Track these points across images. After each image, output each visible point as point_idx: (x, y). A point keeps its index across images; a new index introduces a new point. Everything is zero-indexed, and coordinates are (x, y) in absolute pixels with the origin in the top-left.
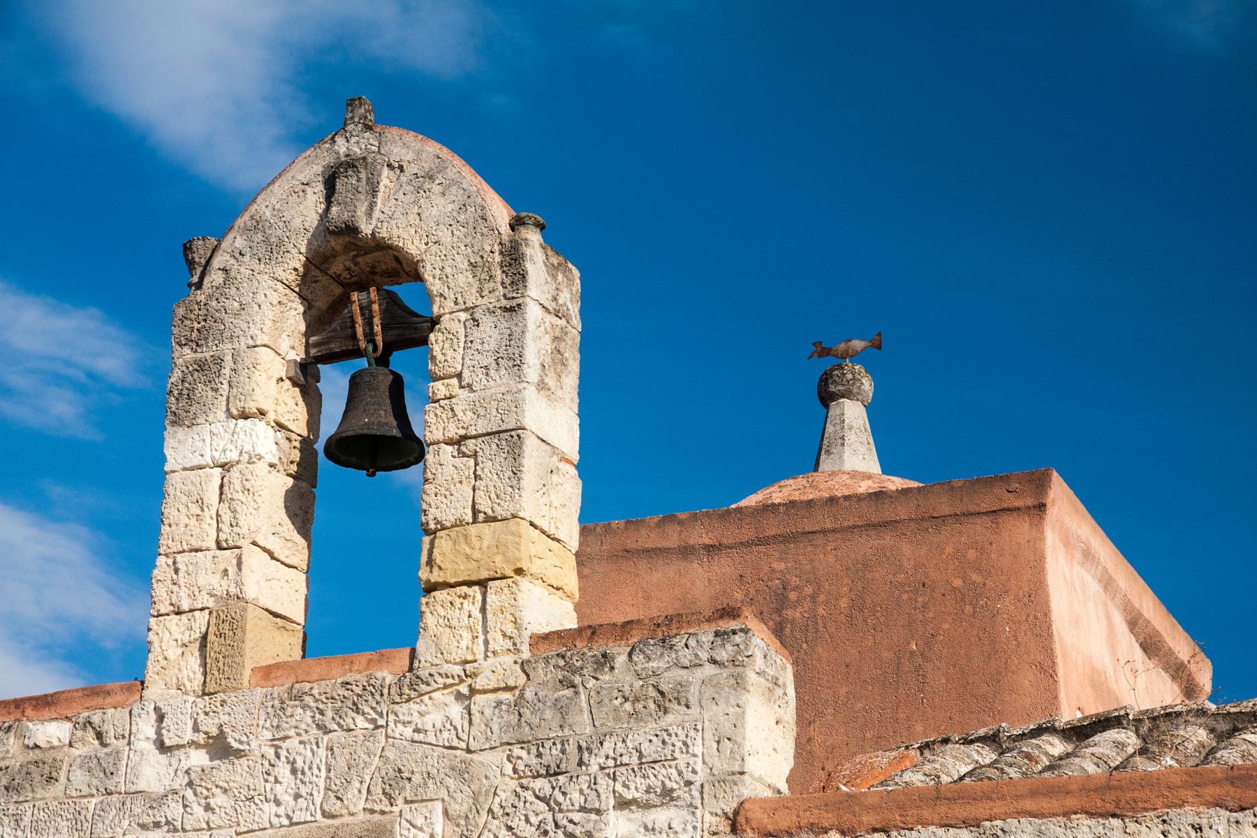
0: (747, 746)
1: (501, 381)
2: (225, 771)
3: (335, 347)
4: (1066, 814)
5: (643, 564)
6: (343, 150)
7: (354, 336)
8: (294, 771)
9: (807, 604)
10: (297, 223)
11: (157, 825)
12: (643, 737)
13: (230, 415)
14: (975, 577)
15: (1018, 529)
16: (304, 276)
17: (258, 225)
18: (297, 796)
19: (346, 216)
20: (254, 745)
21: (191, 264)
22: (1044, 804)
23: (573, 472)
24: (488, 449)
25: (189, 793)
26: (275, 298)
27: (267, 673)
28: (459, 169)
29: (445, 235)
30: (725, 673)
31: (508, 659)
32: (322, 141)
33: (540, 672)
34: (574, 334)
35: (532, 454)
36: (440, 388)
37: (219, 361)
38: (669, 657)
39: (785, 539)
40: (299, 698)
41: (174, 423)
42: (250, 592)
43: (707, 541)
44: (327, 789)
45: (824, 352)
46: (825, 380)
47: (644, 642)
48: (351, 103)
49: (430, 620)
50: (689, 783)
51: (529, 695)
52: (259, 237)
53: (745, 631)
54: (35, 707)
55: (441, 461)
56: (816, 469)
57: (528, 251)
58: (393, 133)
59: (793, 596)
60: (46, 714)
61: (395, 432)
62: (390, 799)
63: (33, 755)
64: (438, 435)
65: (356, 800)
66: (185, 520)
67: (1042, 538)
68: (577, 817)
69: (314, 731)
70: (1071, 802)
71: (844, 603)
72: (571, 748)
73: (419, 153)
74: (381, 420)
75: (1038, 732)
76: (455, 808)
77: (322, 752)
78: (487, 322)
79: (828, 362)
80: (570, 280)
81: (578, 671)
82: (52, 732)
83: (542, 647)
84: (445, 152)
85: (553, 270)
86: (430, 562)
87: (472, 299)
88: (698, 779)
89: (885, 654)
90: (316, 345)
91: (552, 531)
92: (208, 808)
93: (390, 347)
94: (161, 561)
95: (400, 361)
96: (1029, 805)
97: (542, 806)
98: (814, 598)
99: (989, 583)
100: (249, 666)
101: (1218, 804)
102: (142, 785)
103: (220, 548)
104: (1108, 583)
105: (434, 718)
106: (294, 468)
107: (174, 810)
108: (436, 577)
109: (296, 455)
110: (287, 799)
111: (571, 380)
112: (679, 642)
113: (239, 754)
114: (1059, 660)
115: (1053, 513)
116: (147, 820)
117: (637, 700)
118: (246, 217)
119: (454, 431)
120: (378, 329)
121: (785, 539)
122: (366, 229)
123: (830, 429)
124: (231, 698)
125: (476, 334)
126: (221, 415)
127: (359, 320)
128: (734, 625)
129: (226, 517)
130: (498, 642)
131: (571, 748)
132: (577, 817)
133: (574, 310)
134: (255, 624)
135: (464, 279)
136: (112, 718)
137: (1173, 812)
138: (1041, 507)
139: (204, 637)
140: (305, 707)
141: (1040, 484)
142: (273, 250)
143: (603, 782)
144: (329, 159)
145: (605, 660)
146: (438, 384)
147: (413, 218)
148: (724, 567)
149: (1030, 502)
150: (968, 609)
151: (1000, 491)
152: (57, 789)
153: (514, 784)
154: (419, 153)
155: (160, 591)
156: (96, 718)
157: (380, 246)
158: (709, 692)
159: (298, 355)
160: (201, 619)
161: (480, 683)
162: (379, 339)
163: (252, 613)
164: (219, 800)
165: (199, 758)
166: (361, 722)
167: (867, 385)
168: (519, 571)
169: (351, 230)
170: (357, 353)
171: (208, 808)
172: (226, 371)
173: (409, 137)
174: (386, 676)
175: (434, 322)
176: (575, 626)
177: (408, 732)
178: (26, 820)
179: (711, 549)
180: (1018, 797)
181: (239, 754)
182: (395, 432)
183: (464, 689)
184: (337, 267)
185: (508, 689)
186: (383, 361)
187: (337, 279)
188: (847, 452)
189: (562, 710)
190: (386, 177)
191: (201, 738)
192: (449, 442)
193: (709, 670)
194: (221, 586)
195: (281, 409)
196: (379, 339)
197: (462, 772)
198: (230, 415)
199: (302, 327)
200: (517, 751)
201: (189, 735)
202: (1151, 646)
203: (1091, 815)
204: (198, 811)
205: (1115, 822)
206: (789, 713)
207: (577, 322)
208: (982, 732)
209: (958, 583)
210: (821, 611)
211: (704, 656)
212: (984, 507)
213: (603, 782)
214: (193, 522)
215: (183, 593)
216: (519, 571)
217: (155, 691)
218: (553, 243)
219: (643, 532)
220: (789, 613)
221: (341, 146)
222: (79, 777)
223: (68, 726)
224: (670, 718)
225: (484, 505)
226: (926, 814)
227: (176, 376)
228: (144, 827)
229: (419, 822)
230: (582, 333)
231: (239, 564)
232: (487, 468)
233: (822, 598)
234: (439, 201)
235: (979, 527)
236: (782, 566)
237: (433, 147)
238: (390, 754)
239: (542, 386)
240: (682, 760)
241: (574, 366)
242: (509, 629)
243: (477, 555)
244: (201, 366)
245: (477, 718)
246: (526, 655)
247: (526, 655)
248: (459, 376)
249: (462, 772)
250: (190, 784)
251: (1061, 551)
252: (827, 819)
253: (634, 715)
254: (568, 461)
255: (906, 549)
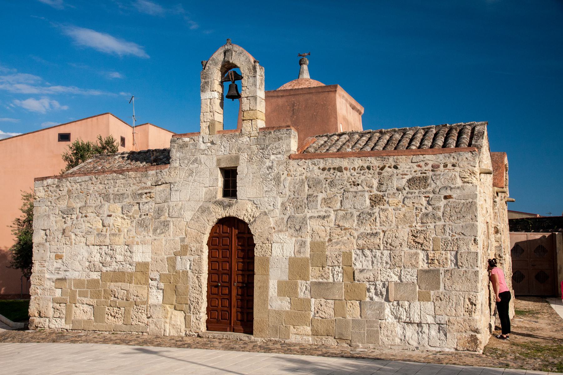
0: (291, 146)
1: (253, 88)
2: (213, 146)
3: (226, 80)
4: (336, 158)
5: (271, 98)
6: (226, 48)
7: (229, 78)
8: (224, 147)
9: (298, 106)
10: (220, 59)
11: (204, 154)
12: (276, 144)
13: (211, 91)
14: (325, 103)
15: (332, 94)
16: (221, 68)
17: (213, 60)
18: (225, 151)
19: (228, 59)
20: (218, 143)
21: (203, 65)
22: (333, 156)
23: (264, 101)
24: (251, 99)
25: (208, 150)
26: (217, 72)
27: (219, 132)
28: (245, 52)
29: (243, 63)
30: (288, 135)
31: (256, 132)
32: (223, 46)
33: (261, 134)
34: (264, 78)
35: (258, 99)
36: (244, 88)
37: (208, 82)
38: (280, 133)
39: (294, 95)
40: (224, 136)
41: (202, 92)
42: (216, 119)
43: (281, 95)
44: (229, 150)
45: (300, 55)
46: (300, 61)
47: (276, 130)
48: (227, 40)
49: (244, 125)
50: (283, 151)
51: (259, 137)
52: (214, 62)
53: (291, 129)
54: (184, 135)
55: (244, 100)
56: (299, 78)
57: (257, 67)
58: (235, 45)
59: (295, 105)
60: (185, 136)
61: (237, 95)
62: (239, 152)
63: (184, 143)
64: (244, 96)
65: (234, 152)
66: (205, 107)
67: (336, 95)
68: (267, 156)
69: (227, 141)
70: (337, 156)
71: (304, 106)
72: (265, 145)
73: (239, 49)
74: (234, 93)
75: (334, 135)
76: (248, 154)
77: (228, 144)
78: (251, 78)
79: (301, 57)
80: (263, 70)
81: (266, 134)
82: (187, 139)
83: (261, 130)
84: (243, 49)
85: (260, 69)
86: (243, 116)
87: (248, 74)
88: (284, 151)
89: (310, 115)
90: (223, 79)
91: (261, 111)
92: (211, 152)
93: (235, 80)
94: (201, 114)
95: (236, 82)
96: (331, 156)
97: (261, 154)
98: (299, 105)
99: (327, 103)
100: (216, 131)
101: (356, 157)
102: (201, 148)
103: (210, 112)
104: (346, 100)
105: (245, 140)
106: (220, 98)
107: (206, 152)
108: (244, 119)
109: (221, 96)
110: (223, 151)
111: (263, 86)
112: (281, 130)
113: (215, 144)
114: (338, 116)
115: (338, 91)
116: (202, 153)
117: (275, 139)
118: (211, 58)
119: (246, 96)
120: (233, 77)
121: (294, 95)
122: (231, 62)
123: (301, 70)
124: (214, 136)
125: (249, 80)
126: (209, 91)
127: (230, 76)
128: (289, 128)
129: (211, 107)
130: (254, 129)
131: (265, 145)
132: (267, 156)
133: (264, 75)
134: (217, 123)
135: (247, 71)
136: (196, 138)
137: (350, 158)
138: (336, 91)
139: (209, 126)
140: (225, 138)
141: (336, 87)
142: (216, 64)
143: (270, 151)
144: (224, 49)
145: (270, 133)
146: (243, 88)
147: (238, 60)
148: (284, 99)
149: (334, 90)
150: (324, 108)
151: (329, 88)
152: (188, 148)
153: (257, 150)
154: (239, 49)
155: (202, 119)
156: (193, 138)
157: (232, 64)
158: (286, 138)
159: (220, 80)
160: (208, 123)
161: (252, 135)
162: (233, 79)
163: (216, 123)
164: (213, 151)
165: (209, 144)
166: (234, 140)
167: (308, 62)
168: (257, 118)
169: (229, 62)
170: (230, 81)
171: (211, 152)
172: (210, 84)
173: (237, 46)
174: (237, 133)
175: (242, 78)
176: (265, 127)
177: (241, 142)
178: (184, 152)
179: (282, 96)
180: (329, 155)
181: (215, 144)
182: (237, 95)
183: (249, 136)
184: (226, 66)
185: (256, 136)
186: (234, 82)
187: (226, 68)
188: (304, 74)
189: (264, 140)
190: (234, 53)
191: (210, 141)
192: (246, 97)
193: (286, 135)
194: (211, 118)
195: (218, 89)
196: (233, 79)
197: (249, 148)
198: (211, 91)
199: (221, 76)
200: (257, 146)
201: (208, 141)
202: (354, 108)
203: (339, 158)
204: (210, 152)
205: (342, 159)
206: (297, 140)
207: (264, 77)
208: (325, 134)
209: (322, 103)
210: (300, 107)
211: (285, 133)
212: (326, 91)
213: (270, 151)
214: (206, 108)
215: (205, 119)
216: (257, 118)
217: (202, 134)
218: (260, 65)
219: (271, 93)
220: (295, 107)
221: (226, 47)
222: (191, 146)
223: (189, 139)
224: (280, 142)
225: (251, 108)
226: (316, 157)
227: (202, 84)
228: (202, 154)
229: (243, 155)
230: (265, 78)
231: (214, 115)
232: (251, 102)
233: (300, 105)
234: (243, 58)
235: (326, 94)
236: (294, 99)
237: (241, 48)
238: (238, 145)
239: (259, 88)
240: (282, 148)
241: (264, 84)
242: (256, 127)
243: (250, 115)
244: (206, 83)
245: (251, 141)
246: (258, 131)
247: (258, 131)
248: (247, 87)
249: (249, 148)
250: (208, 148)
251: (339, 97)
252: (303, 157)
253: (275, 141)
254: (263, 99)
255: (314, 97)
